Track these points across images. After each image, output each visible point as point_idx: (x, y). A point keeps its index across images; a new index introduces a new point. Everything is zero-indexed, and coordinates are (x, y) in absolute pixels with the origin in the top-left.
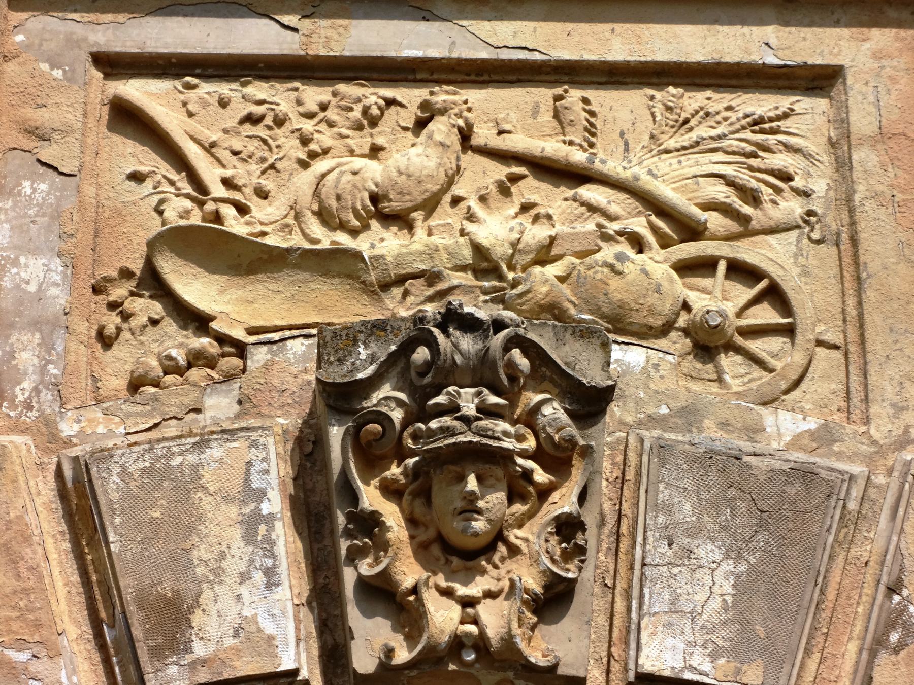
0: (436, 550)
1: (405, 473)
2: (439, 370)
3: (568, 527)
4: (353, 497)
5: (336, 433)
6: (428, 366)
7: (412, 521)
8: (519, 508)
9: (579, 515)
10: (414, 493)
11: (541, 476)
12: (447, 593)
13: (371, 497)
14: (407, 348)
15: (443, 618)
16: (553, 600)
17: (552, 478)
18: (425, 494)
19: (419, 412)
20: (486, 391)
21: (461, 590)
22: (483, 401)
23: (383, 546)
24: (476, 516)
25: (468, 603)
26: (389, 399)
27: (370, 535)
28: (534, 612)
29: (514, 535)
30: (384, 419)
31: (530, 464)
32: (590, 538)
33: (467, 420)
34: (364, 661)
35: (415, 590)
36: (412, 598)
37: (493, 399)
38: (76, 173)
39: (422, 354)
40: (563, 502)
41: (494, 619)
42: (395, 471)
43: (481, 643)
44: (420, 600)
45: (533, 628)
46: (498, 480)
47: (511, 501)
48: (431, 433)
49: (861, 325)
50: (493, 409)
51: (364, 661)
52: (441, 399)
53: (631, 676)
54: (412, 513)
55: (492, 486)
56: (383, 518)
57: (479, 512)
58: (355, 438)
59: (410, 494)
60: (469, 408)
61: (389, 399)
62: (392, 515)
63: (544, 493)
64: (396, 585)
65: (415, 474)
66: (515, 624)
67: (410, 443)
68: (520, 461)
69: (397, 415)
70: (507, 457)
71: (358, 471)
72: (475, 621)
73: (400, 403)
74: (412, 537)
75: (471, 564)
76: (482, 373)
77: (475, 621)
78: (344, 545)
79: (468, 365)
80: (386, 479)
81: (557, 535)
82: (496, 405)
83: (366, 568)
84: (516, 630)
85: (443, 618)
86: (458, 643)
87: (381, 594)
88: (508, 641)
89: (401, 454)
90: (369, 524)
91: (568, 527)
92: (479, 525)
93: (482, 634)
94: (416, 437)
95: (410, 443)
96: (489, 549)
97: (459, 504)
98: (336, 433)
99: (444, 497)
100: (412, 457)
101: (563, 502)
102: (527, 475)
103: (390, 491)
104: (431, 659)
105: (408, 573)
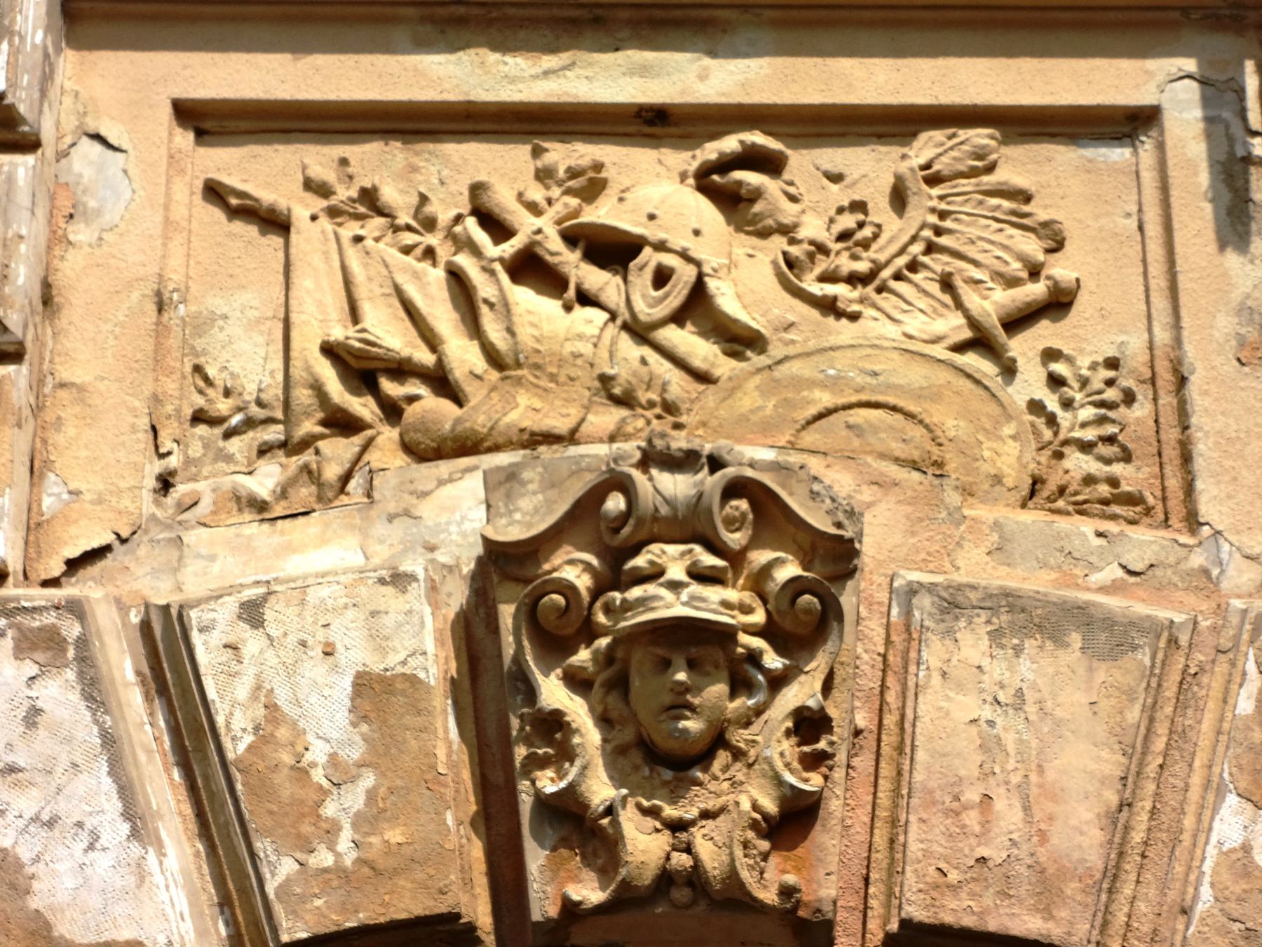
0: (636, 756)
1: (595, 659)
2: (640, 522)
3: (809, 725)
4: (531, 693)
5: (507, 613)
6: (625, 517)
7: (604, 721)
8: (744, 702)
9: (822, 709)
10: (609, 686)
11: (773, 661)
12: (653, 812)
13: (553, 692)
14: (596, 495)
15: (644, 845)
16: (793, 821)
17: (787, 662)
18: (620, 684)
19: (615, 575)
20: (698, 549)
21: (670, 811)
22: (694, 564)
23: (566, 753)
24: (688, 714)
25: (678, 826)
26: (573, 568)
27: (550, 742)
28: (762, 835)
29: (739, 737)
30: (568, 589)
31: (757, 643)
32: (835, 741)
33: (675, 586)
34: (543, 904)
35: (610, 811)
36: (605, 821)
37: (709, 560)
38: (85, 140)
39: (615, 503)
40: (801, 693)
41: (709, 850)
42: (583, 656)
43: (695, 877)
44: (616, 824)
45: (765, 857)
46: (717, 667)
47: (733, 695)
48: (627, 606)
49: (1186, 458)
50: (707, 572)
51: (543, 904)
52: (640, 561)
53: (894, 926)
54: (605, 710)
55: (708, 674)
56: (567, 719)
57: (692, 709)
58: (531, 615)
59: (602, 685)
60: (676, 572)
61: (573, 568)
62: (577, 710)
63: (777, 682)
64: (586, 807)
65: (608, 658)
66: (739, 852)
67: (601, 618)
68: (744, 638)
69: (583, 582)
70: (725, 635)
71: (535, 659)
72: (688, 850)
73: (588, 567)
74: (605, 740)
75: (682, 774)
76: (690, 526)
77: (688, 850)
78: (521, 752)
79: (675, 516)
80: (570, 666)
81: (796, 735)
82: (713, 567)
83: (548, 783)
84: (742, 862)
85: (644, 845)
86: (666, 878)
87: (574, 824)
88: (732, 875)
89: (589, 632)
90: (553, 726)
91: (809, 725)
92: (692, 725)
93: (697, 865)
94: (608, 609)
95: (601, 618)
96: (704, 758)
97: (667, 699)
98: (507, 613)
99: (646, 690)
100: (605, 635)
101: (801, 693)
102: (754, 658)
103: (577, 682)
104: (627, 899)
105: (600, 790)
